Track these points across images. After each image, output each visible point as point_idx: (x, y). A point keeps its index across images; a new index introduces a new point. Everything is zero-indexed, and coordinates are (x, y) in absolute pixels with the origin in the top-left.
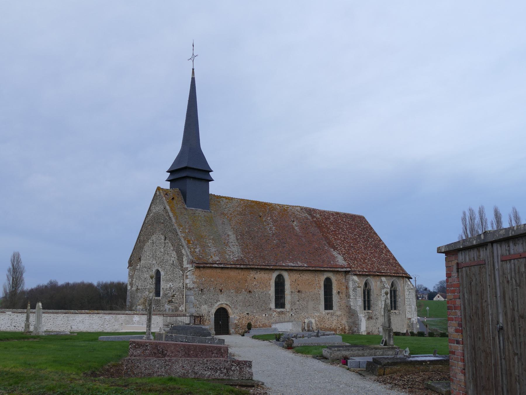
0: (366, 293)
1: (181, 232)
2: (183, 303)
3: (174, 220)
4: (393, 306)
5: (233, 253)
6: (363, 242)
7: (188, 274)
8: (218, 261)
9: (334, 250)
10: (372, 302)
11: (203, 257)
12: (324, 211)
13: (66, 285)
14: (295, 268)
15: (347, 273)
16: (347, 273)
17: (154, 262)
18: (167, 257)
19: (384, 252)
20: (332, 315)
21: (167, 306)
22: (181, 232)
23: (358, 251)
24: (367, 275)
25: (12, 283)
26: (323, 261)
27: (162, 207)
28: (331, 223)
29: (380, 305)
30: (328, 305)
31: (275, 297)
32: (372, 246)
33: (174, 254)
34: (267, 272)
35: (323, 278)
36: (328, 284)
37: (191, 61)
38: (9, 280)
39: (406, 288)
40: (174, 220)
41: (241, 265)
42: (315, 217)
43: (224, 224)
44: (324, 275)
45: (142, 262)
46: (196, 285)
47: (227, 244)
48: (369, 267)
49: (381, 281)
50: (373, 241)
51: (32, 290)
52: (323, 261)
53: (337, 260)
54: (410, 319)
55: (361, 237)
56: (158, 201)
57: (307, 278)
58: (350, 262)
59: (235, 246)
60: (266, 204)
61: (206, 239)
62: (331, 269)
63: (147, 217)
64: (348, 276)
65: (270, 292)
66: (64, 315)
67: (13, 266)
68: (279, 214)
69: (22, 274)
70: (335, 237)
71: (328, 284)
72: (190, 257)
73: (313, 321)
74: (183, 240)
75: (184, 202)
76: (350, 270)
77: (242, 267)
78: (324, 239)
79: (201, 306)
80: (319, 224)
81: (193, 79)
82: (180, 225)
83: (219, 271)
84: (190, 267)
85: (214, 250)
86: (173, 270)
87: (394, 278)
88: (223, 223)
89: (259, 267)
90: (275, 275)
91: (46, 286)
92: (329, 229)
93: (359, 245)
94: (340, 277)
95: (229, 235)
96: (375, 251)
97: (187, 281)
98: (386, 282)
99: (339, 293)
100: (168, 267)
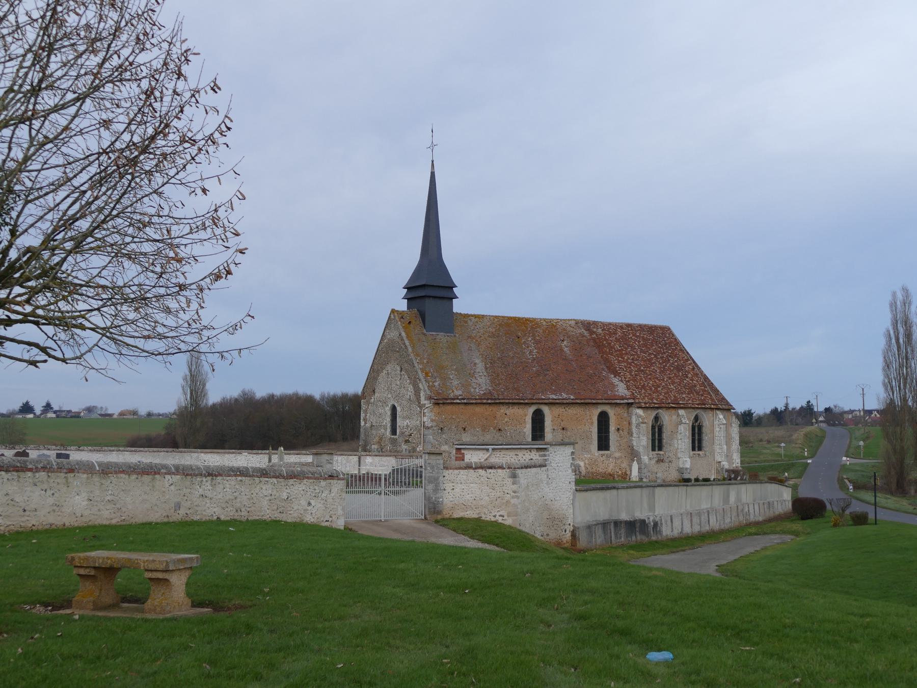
0: (657, 430)
1: (418, 363)
2: (420, 443)
3: (410, 350)
4: (697, 445)
5: (479, 385)
6: (660, 364)
7: (425, 411)
8: (460, 395)
9: (615, 377)
10: (665, 441)
11: (443, 392)
12: (610, 324)
13: (269, 398)
14: (557, 401)
15: (629, 405)
16: (629, 405)
17: (390, 396)
18: (403, 391)
19: (690, 376)
20: (608, 457)
21: (404, 447)
22: (418, 363)
23: (649, 377)
24: (658, 408)
25: (191, 399)
26: (598, 391)
27: (398, 333)
28: (617, 340)
29: (676, 445)
30: (603, 444)
31: (532, 435)
32: (672, 368)
33: (411, 388)
34: (521, 406)
35: (596, 412)
36: (603, 420)
37: (430, 150)
38: (185, 394)
39: (716, 423)
40: (410, 350)
41: (488, 399)
42: (594, 332)
43: (471, 350)
44: (597, 408)
45: (376, 395)
46: (435, 424)
47: (472, 375)
48: (661, 397)
49: (678, 415)
50: (676, 361)
51: (214, 405)
52: (598, 391)
53: (616, 389)
54: (720, 462)
55: (659, 357)
56: (393, 325)
57: (575, 412)
58: (634, 392)
59: (482, 377)
60: (527, 320)
61: (448, 369)
62: (607, 402)
63: (380, 343)
64: (630, 409)
65: (525, 430)
66: (296, 456)
67: (190, 371)
68: (544, 332)
69: (204, 385)
70: (620, 359)
71: (603, 420)
72: (428, 393)
73: (582, 464)
74: (419, 372)
75: (422, 326)
76: (633, 401)
77: (489, 401)
78: (603, 362)
79: (440, 446)
80: (598, 343)
81: (433, 175)
82: (418, 355)
83: (462, 406)
84: (427, 403)
85: (456, 383)
86: (410, 406)
87: (698, 411)
88: (470, 349)
89: (511, 401)
90: (532, 410)
91: (236, 400)
92: (613, 347)
93: (652, 368)
94: (621, 411)
95: (475, 364)
96: (675, 374)
97: (425, 419)
98: (686, 417)
99: (618, 429)
100: (405, 403)
